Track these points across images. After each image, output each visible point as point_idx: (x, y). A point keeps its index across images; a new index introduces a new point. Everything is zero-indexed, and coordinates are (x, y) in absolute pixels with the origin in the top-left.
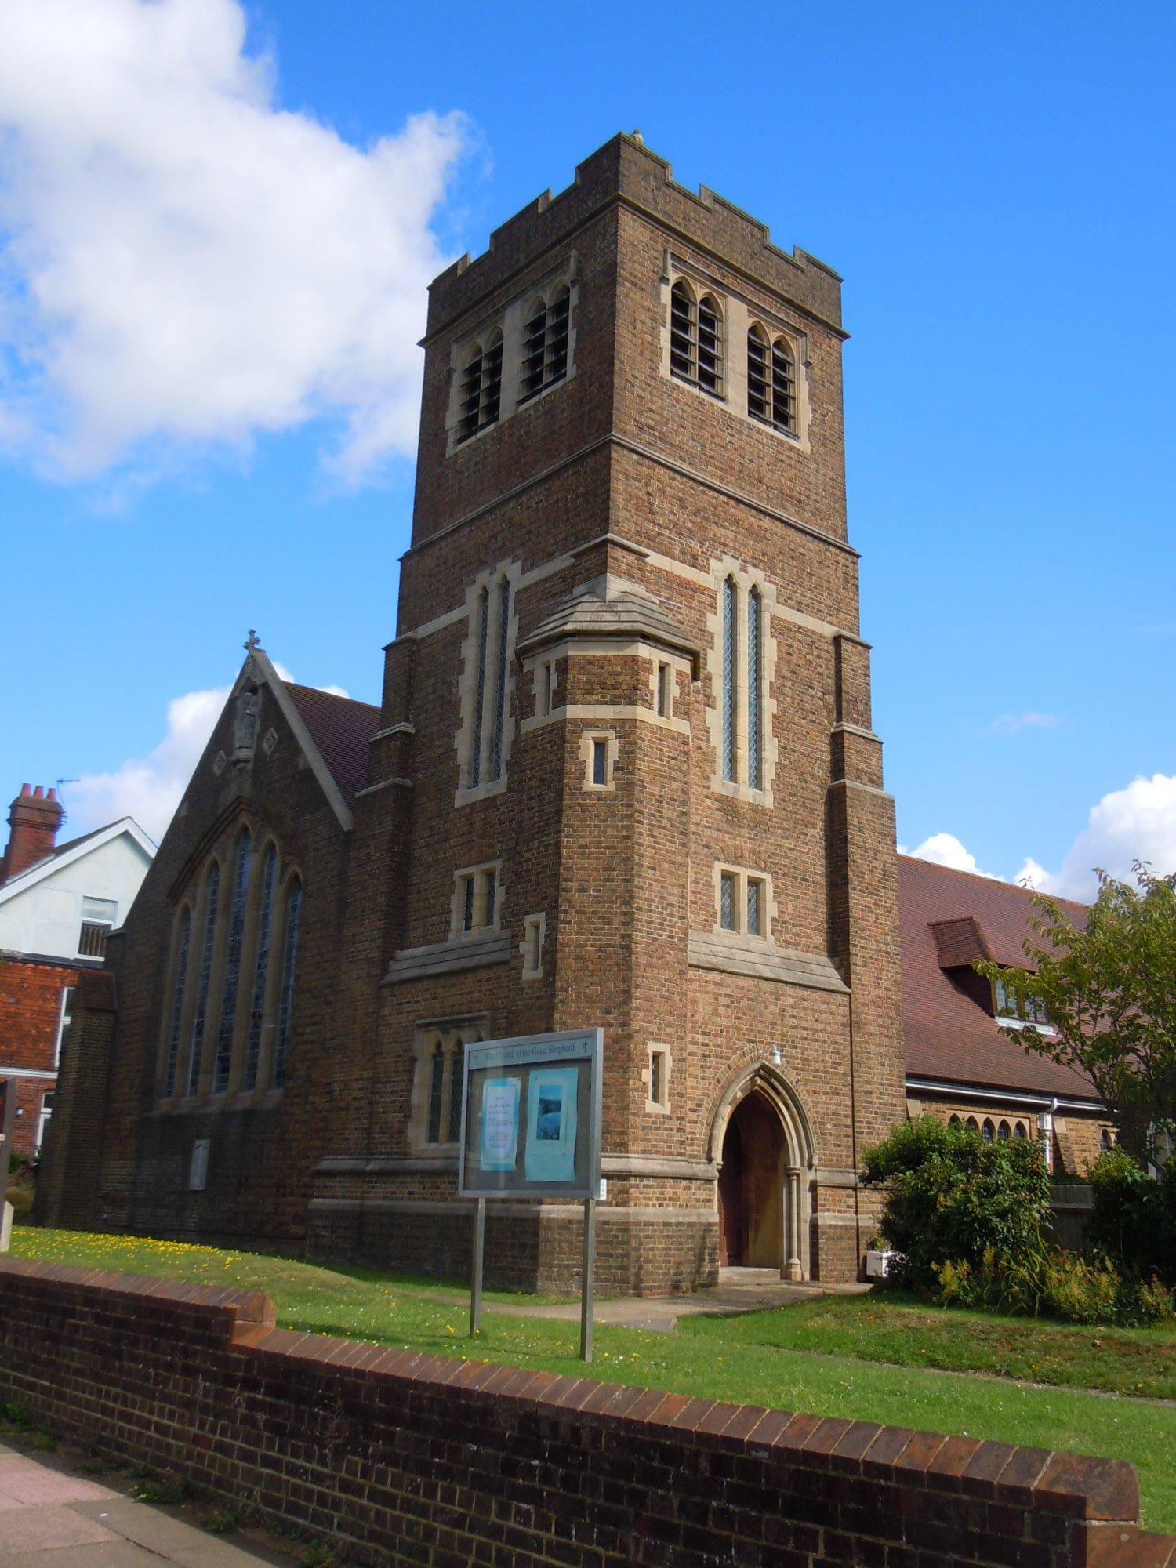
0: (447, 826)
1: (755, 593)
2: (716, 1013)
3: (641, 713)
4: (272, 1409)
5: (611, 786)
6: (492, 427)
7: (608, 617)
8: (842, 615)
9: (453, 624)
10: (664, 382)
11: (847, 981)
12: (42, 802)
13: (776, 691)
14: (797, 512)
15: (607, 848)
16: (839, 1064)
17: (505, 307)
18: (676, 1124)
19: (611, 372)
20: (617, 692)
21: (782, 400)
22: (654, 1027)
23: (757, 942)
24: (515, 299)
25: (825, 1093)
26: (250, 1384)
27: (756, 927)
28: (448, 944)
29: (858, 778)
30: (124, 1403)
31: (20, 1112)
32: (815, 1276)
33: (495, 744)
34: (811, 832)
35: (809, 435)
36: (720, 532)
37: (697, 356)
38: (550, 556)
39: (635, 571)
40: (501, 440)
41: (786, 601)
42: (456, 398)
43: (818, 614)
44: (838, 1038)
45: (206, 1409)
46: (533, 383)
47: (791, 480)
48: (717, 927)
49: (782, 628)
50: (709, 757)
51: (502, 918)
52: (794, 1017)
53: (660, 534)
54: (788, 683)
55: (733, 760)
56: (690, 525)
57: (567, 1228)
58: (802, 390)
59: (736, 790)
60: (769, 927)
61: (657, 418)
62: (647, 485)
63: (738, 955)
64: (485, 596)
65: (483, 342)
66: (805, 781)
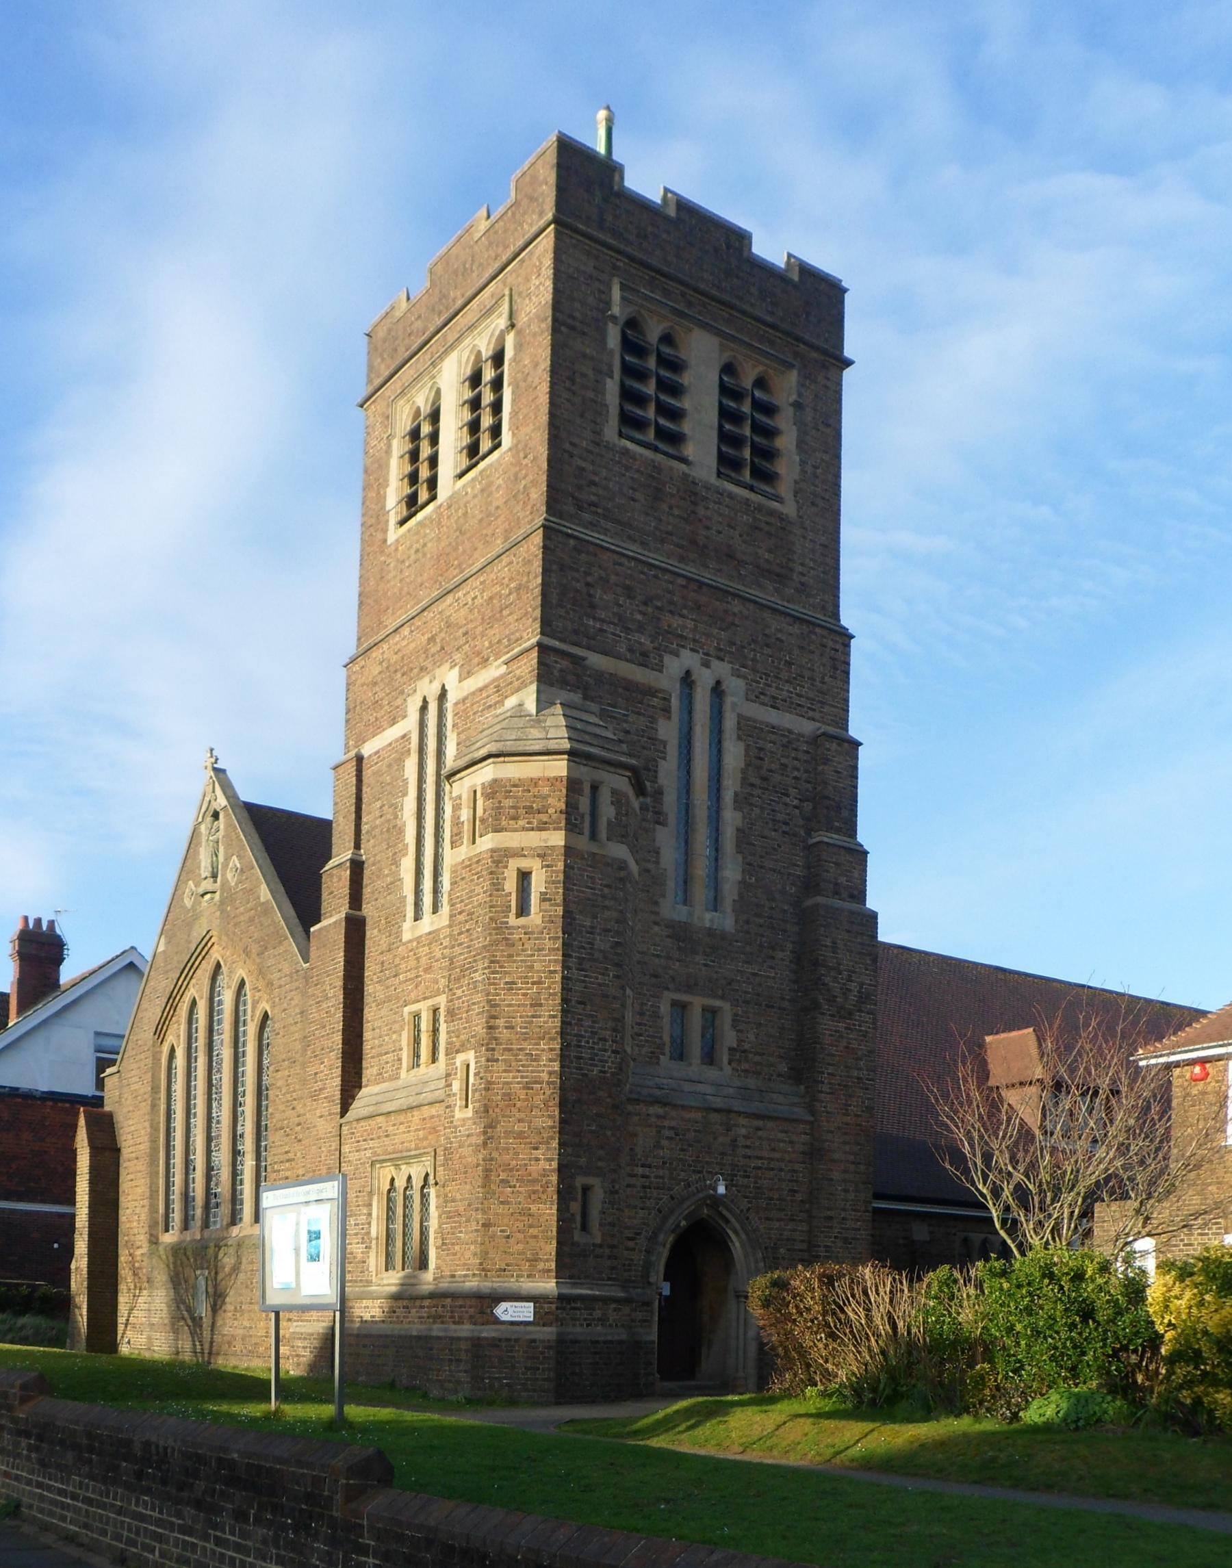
0: (397, 961)
1: (718, 691)
2: (658, 1146)
9: (397, 741)
10: (610, 448)
11: (812, 1111)
12: (43, 933)
14: (776, 590)
15: (533, 983)
17: (441, 358)
18: (607, 1251)
20: (544, 818)
22: (583, 1161)
23: (712, 1073)
24: (452, 347)
25: (779, 1220)
27: (710, 1058)
28: (400, 1083)
29: (836, 893)
31: (56, 1246)
34: (780, 955)
35: (796, 494)
36: (676, 622)
38: (485, 662)
40: (439, 523)
41: (755, 696)
47: (770, 551)
49: (748, 729)
52: (747, 1147)
53: (601, 630)
55: (687, 881)
56: (639, 617)
57: (497, 1346)
58: (786, 441)
59: (691, 914)
62: (587, 574)
63: (687, 1087)
64: (424, 708)
65: (422, 400)
66: (774, 900)
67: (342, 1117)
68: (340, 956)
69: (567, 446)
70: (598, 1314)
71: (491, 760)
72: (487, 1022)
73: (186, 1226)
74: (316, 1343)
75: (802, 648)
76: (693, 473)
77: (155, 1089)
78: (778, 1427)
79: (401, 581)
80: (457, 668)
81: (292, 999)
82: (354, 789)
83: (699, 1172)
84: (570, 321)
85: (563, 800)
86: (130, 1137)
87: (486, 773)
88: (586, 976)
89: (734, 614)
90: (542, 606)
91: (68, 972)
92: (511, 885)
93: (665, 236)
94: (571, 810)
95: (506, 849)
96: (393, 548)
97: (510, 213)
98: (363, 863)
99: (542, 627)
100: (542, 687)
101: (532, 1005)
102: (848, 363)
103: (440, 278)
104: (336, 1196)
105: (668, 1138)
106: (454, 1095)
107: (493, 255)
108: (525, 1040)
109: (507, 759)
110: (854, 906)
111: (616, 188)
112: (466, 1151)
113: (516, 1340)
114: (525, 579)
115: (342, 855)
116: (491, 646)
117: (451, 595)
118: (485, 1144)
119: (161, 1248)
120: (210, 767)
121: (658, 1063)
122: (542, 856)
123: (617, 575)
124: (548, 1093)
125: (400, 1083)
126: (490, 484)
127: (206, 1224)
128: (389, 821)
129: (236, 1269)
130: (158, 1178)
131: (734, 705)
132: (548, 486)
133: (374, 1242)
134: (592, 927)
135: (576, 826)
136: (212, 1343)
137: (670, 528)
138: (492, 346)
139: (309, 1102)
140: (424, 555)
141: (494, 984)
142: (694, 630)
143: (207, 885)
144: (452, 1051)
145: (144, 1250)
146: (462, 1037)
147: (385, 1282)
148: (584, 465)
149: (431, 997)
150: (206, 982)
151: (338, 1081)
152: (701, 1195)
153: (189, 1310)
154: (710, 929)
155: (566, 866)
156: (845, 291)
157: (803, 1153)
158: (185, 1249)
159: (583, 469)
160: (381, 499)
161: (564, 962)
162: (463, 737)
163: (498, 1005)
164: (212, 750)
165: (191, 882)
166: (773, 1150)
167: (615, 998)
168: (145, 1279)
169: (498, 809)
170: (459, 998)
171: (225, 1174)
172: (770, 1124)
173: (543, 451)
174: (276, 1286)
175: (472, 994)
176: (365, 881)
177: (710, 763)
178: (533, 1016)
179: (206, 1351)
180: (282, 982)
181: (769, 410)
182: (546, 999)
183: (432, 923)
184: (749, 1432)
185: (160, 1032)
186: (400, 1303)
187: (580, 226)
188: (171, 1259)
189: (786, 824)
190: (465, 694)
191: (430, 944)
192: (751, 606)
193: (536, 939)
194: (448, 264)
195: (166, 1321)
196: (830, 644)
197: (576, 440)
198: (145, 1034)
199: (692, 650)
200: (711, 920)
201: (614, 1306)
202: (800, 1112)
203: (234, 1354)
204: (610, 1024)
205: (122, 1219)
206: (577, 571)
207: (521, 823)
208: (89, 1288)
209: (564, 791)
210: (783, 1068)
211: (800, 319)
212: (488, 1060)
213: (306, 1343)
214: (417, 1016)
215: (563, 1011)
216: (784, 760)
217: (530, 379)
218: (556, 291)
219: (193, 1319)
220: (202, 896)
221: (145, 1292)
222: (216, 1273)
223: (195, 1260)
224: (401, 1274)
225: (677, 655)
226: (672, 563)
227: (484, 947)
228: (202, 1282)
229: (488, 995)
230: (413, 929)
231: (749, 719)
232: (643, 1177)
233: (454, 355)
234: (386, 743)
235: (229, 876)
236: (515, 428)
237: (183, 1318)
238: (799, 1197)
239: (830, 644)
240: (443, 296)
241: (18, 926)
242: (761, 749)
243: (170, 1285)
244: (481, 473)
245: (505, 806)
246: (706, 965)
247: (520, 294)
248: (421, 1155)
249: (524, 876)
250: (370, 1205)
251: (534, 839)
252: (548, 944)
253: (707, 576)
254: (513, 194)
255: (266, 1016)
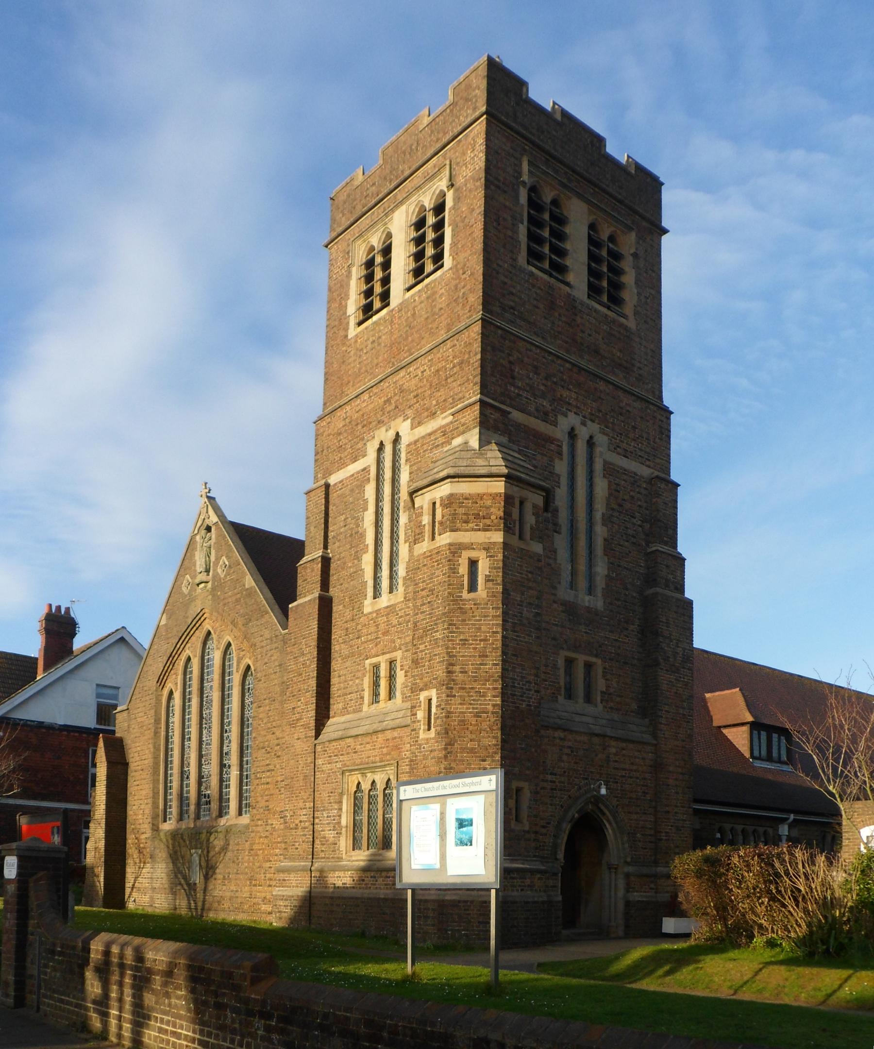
0: (359, 627)
1: (591, 443)
4: (282, 1032)
6: (385, 311)
8: (658, 461)
9: (358, 472)
10: (522, 270)
11: (655, 736)
15: (481, 640)
16: (647, 793)
17: (393, 211)
18: (533, 836)
20: (488, 522)
21: (616, 286)
23: (590, 709)
24: (401, 203)
25: (637, 813)
26: (265, 1015)
29: (667, 586)
30: (174, 1026)
34: (632, 627)
35: (635, 314)
36: (566, 393)
38: (433, 415)
39: (500, 425)
40: (392, 322)
41: (615, 448)
44: (648, 776)
45: (234, 1031)
47: (620, 351)
48: (561, 699)
49: (610, 470)
51: (403, 694)
52: (616, 761)
53: (519, 395)
54: (616, 514)
56: (542, 388)
58: (629, 278)
61: (517, 299)
62: (509, 355)
64: (381, 448)
65: (376, 240)
66: (627, 589)
67: (316, 739)
68: (314, 625)
69: (495, 266)
70: (528, 882)
71: (449, 480)
72: (447, 668)
73: (181, 818)
74: (296, 903)
75: (642, 418)
76: (573, 294)
77: (157, 721)
78: (756, 973)
79: (360, 363)
80: (409, 421)
81: (272, 656)
82: (323, 508)
83: (586, 779)
84: (495, 181)
85: (502, 509)
86: (136, 755)
87: (445, 490)
88: (517, 636)
89: (601, 391)
90: (481, 374)
91: (78, 643)
92: (463, 569)
93: (554, 133)
94: (507, 516)
95: (460, 544)
96: (353, 341)
97: (448, 111)
98: (330, 559)
99: (481, 389)
100: (482, 431)
101: (480, 656)
102: (665, 231)
103: (391, 157)
104: (493, 787)
105: (567, 754)
106: (419, 721)
107: (435, 139)
108: (475, 681)
109: (460, 479)
110: (678, 595)
111: (524, 97)
112: (430, 762)
113: (472, 902)
114: (467, 356)
115: (313, 554)
116: (438, 403)
117: (404, 370)
118: (446, 757)
119: (162, 834)
120: (204, 496)
121: (557, 701)
122: (487, 549)
123: (528, 357)
124: (493, 720)
125: (363, 714)
126: (434, 293)
127: (198, 817)
128: (352, 528)
129: (225, 849)
130: (158, 783)
131: (601, 453)
132: (483, 292)
133: (344, 830)
134: (521, 601)
135: (510, 528)
136: (204, 901)
137: (560, 329)
138: (433, 201)
139: (287, 729)
140: (379, 344)
141: (451, 640)
142: (577, 399)
143: (203, 577)
144: (415, 689)
145: (148, 835)
146: (425, 680)
147: (354, 858)
148: (506, 280)
149: (389, 652)
150: (199, 646)
151: (313, 713)
152: (589, 795)
153: (185, 878)
154: (588, 607)
155: (504, 556)
156: (662, 184)
157: (651, 766)
158: (182, 834)
159: (505, 283)
160: (343, 308)
161: (503, 625)
162: (415, 468)
163: (455, 656)
164: (206, 484)
165: (188, 576)
166: (632, 764)
167: (536, 652)
168: (148, 856)
169: (454, 515)
170: (421, 651)
171: (214, 781)
172: (631, 746)
173: (479, 269)
174: (413, 867)
175: (434, 648)
176: (332, 572)
177: (587, 495)
178: (481, 664)
179: (199, 908)
180: (264, 644)
181: (616, 256)
182: (490, 652)
183: (389, 600)
184: (723, 975)
185: (161, 681)
186: (368, 874)
187: (503, 118)
188: (170, 842)
189: (633, 536)
190: (416, 438)
191: (388, 614)
192: (611, 387)
193: (483, 608)
194: (397, 147)
195: (166, 886)
196: (659, 417)
197: (500, 263)
198: (151, 682)
199: (575, 413)
200: (589, 601)
201: (539, 876)
202: (647, 737)
203: (224, 910)
204: (533, 671)
205: (130, 812)
206: (503, 352)
207: (470, 525)
208: (106, 862)
209: (503, 503)
210: (634, 706)
211: (634, 200)
212: (448, 696)
213: (287, 903)
214: (376, 667)
215: (503, 660)
216: (632, 493)
217: (467, 220)
218: (487, 160)
219: (189, 885)
220: (198, 585)
221: (148, 865)
222: (208, 852)
223: (191, 842)
224: (367, 853)
225: (566, 416)
226: (562, 353)
227: (444, 614)
228: (196, 858)
229: (447, 648)
230: (372, 604)
231: (611, 464)
232: (551, 782)
233: (403, 208)
234: (349, 475)
235: (219, 571)
236: (454, 254)
237: (180, 884)
238: (648, 797)
239: (659, 417)
240: (393, 170)
241: (44, 611)
242: (617, 485)
243: (169, 860)
244: (427, 286)
245: (458, 513)
246: (586, 633)
247: (458, 164)
248: (385, 766)
250: (340, 802)
251: (481, 537)
252: (492, 612)
253: (583, 363)
254: (451, 97)
255: (248, 668)
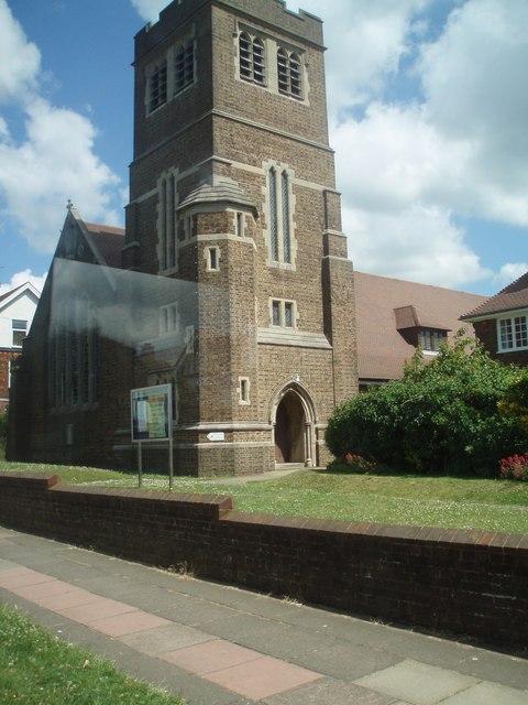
1: (284, 175)
3: (230, 236)
5: (218, 269)
7: (214, 194)
13: (295, 219)
19: (211, 81)
21: (295, 83)
23: (289, 330)
32: (318, 465)
33: (173, 251)
37: (252, 68)
41: (299, 176)
42: (148, 91)
43: (315, 181)
44: (328, 368)
46: (180, 84)
49: (297, 189)
50: (263, 250)
58: (305, 77)
60: (295, 323)
64: (164, 184)
65: (158, 63)
202: (329, 346)
241: (89, 153)
249: (213, 252)
